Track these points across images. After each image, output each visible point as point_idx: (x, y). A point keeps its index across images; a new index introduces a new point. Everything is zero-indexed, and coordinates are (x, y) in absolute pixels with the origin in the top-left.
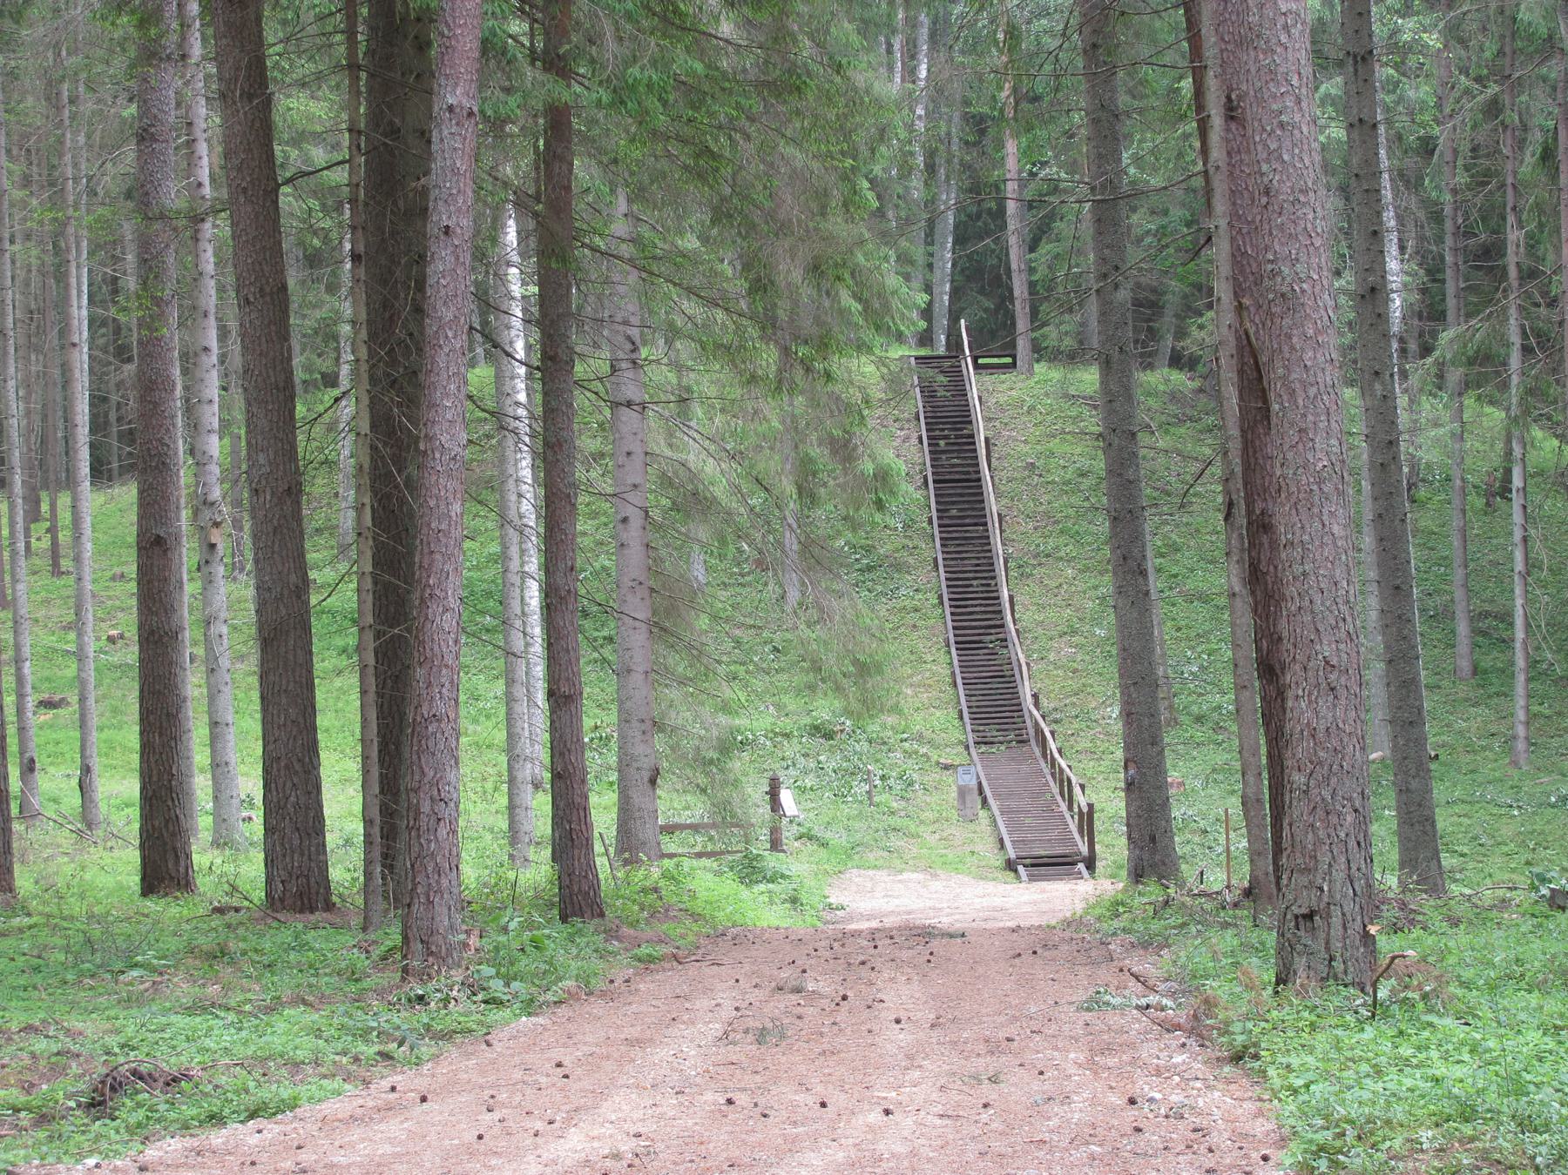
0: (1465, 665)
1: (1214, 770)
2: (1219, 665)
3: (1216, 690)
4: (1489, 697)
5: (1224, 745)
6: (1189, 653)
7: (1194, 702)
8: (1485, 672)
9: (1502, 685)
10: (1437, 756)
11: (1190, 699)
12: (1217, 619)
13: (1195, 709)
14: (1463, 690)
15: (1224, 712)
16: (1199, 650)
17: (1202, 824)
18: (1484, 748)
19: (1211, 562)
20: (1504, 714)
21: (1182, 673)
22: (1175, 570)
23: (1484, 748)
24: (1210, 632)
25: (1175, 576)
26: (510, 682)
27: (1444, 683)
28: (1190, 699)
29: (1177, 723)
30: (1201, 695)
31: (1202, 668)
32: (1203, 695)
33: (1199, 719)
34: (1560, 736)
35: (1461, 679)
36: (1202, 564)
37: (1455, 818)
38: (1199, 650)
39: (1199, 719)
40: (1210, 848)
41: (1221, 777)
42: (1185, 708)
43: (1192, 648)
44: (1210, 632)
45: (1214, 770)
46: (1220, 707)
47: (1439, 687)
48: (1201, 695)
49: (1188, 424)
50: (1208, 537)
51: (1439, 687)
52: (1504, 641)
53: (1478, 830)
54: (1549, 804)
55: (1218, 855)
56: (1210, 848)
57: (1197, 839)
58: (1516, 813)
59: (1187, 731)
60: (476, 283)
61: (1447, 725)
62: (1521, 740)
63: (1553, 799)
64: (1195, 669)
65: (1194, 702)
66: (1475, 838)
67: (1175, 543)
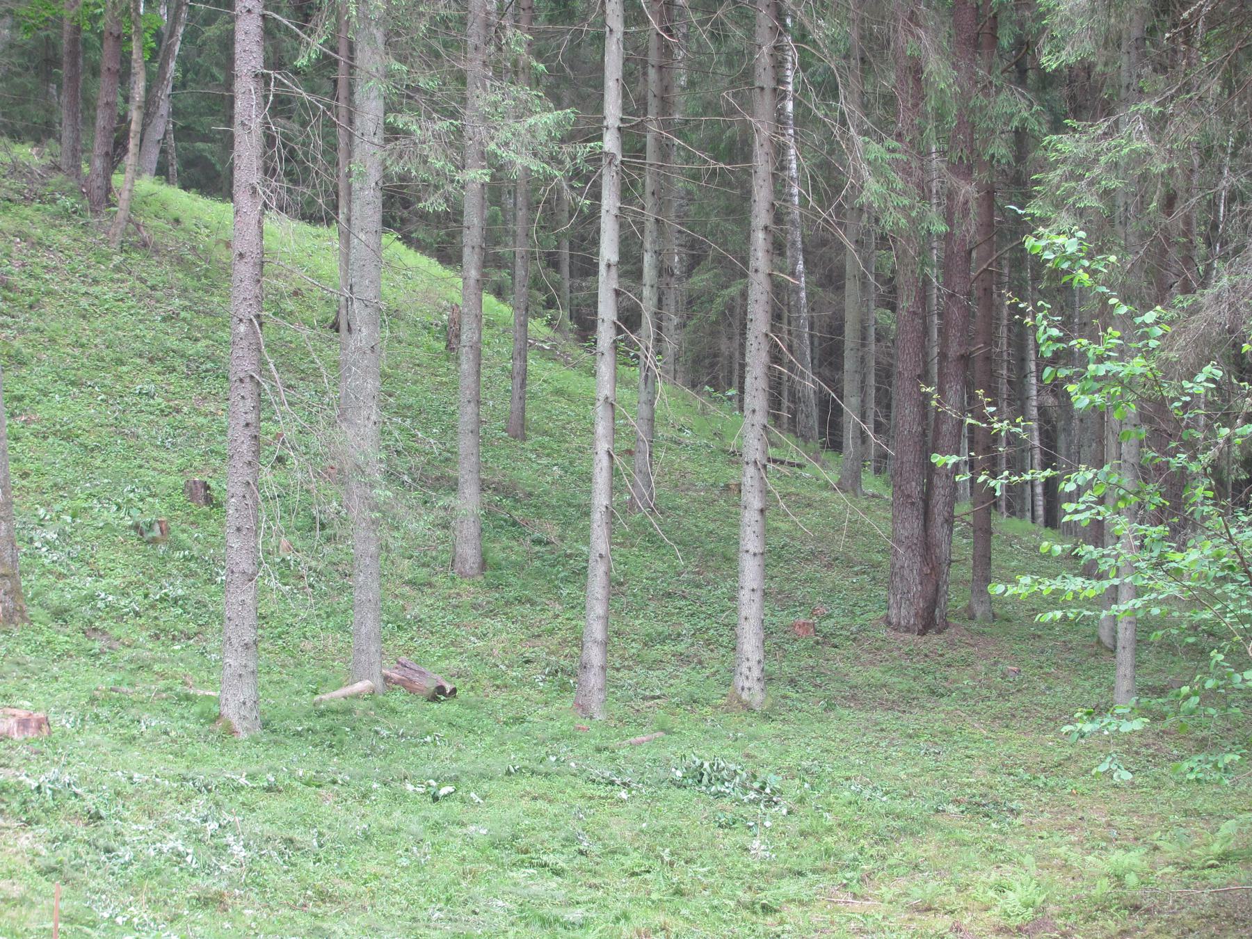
0: (469, 553)
1: (93, 700)
2: (90, 532)
3: (85, 570)
4: (508, 603)
5: (105, 658)
6: (42, 512)
7: (51, 587)
8: (498, 566)
9: (524, 587)
10: (454, 691)
11: (45, 582)
12: (84, 464)
13: (53, 597)
14: (468, 591)
15: (101, 604)
16: (57, 507)
17: (91, 802)
18: (521, 682)
19: (73, 383)
20: (536, 631)
21: (31, 540)
22: (19, 390)
23: (521, 682)
24: (74, 482)
25: (20, 399)
26: (523, 416)
27: (438, 579)
28: (45, 582)
29: (24, 619)
30: (61, 576)
31: (62, 534)
32: (65, 576)
33: (60, 614)
34: (630, 668)
35: (463, 575)
36: (60, 385)
37: (525, 804)
38: (57, 507)
39: (60, 614)
40: (108, 850)
41: (104, 712)
42: (37, 595)
43: (47, 505)
44: (74, 482)
45: (93, 700)
46: (92, 597)
47: (430, 585)
48: (61, 576)
49: (36, 205)
50: (69, 350)
51: (430, 585)
52: (514, 524)
53: (574, 826)
54: (673, 782)
55: (126, 866)
56: (108, 850)
57: (81, 831)
58: (624, 794)
59: (40, 632)
60: (193, 908)
61: (452, 643)
62: (596, 670)
63: (679, 774)
64: (51, 536)
65: (51, 587)
66: (569, 840)
67: (19, 352)
